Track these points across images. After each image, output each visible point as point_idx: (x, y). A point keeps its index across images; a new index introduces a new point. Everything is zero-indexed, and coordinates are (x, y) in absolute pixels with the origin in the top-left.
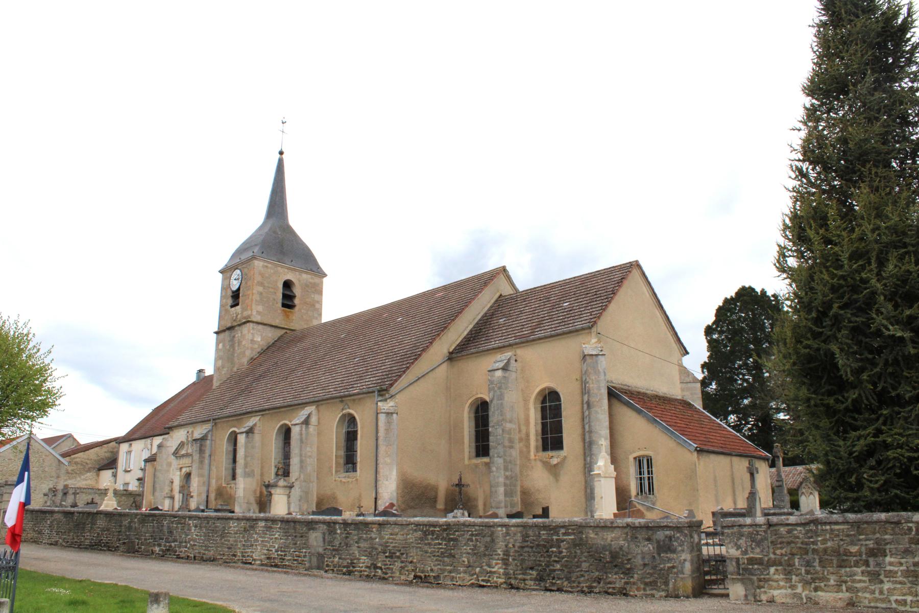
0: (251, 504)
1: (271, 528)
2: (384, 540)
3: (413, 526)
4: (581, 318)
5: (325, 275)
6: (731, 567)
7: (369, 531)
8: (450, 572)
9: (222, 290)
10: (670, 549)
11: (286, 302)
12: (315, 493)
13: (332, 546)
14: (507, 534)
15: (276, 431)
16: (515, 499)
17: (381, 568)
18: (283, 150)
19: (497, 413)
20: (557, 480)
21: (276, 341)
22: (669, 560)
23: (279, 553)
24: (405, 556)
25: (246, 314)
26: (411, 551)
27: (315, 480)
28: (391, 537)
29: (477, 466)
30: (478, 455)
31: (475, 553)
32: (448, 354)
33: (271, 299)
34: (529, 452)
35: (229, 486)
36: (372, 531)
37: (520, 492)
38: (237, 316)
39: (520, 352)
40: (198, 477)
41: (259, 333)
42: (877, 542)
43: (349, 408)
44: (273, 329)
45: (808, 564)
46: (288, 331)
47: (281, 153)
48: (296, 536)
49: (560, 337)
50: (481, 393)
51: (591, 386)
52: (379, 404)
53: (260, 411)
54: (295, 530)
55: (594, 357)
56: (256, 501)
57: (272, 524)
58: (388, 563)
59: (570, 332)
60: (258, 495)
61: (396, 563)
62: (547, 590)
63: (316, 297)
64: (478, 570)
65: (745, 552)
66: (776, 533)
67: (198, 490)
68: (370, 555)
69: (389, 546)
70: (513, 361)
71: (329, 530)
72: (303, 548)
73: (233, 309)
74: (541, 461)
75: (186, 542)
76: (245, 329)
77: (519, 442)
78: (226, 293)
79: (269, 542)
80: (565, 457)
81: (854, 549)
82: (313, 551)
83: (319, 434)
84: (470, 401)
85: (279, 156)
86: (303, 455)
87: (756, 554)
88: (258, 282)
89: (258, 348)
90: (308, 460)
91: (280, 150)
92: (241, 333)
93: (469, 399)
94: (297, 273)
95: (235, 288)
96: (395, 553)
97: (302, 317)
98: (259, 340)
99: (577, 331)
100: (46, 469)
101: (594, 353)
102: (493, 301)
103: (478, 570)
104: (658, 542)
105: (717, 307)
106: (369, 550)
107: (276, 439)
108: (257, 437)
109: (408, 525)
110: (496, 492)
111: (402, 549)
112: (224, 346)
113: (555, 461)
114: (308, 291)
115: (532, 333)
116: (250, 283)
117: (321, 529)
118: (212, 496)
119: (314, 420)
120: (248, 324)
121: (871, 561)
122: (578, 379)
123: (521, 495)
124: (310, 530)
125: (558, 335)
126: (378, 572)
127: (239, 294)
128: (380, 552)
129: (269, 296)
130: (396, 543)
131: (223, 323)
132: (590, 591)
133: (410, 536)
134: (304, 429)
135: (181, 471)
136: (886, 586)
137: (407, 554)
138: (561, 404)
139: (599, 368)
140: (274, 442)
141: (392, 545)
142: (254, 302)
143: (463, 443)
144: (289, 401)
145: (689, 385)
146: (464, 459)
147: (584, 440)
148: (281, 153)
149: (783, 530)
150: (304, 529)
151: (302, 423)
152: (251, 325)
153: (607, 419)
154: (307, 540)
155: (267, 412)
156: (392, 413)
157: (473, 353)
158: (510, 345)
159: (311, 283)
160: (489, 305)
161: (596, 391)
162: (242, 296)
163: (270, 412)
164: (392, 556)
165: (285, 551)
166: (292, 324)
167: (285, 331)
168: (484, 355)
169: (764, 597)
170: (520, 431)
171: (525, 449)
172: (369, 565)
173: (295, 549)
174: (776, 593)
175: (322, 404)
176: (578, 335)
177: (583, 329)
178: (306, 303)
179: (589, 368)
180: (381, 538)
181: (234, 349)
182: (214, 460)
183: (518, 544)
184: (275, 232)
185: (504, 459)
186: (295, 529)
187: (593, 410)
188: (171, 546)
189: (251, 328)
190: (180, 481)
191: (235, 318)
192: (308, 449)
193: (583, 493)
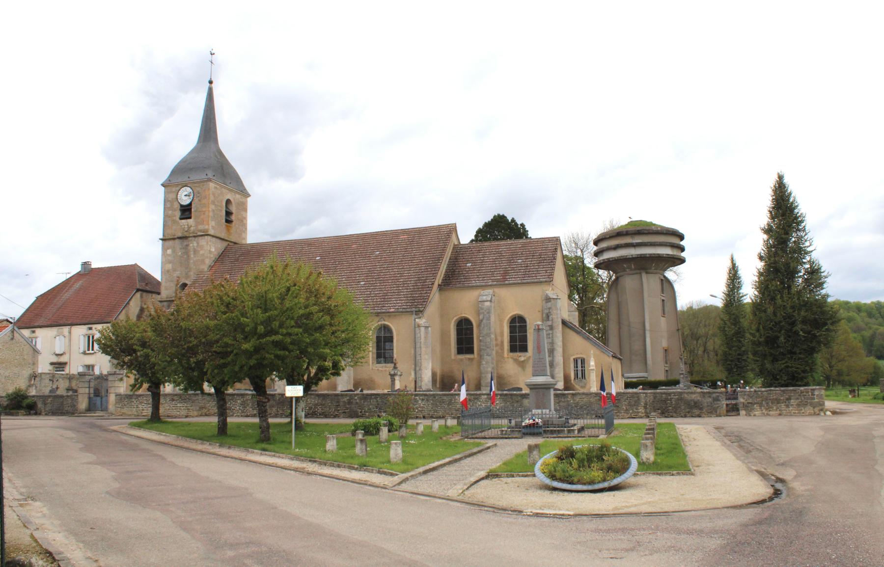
5: (249, 196)
6: (741, 405)
8: (616, 413)
10: (718, 400)
14: (646, 396)
18: (212, 79)
19: (486, 328)
20: (524, 370)
22: (718, 404)
25: (201, 227)
29: (462, 360)
30: (460, 351)
31: (630, 404)
34: (503, 353)
39: (497, 290)
42: (789, 396)
44: (221, 241)
45: (767, 403)
46: (230, 244)
47: (211, 82)
52: (417, 320)
62: (666, 417)
64: (631, 411)
65: (746, 400)
66: (757, 394)
74: (512, 358)
76: (203, 241)
81: (782, 398)
84: (455, 318)
87: (750, 401)
91: (209, 79)
92: (198, 243)
99: (541, 282)
100: (25, 357)
103: (631, 411)
104: (713, 398)
105: (477, 229)
110: (486, 377)
112: (174, 252)
113: (522, 359)
116: (204, 201)
120: (206, 237)
121: (787, 402)
127: (191, 209)
131: (169, 231)
132: (685, 416)
136: (791, 408)
142: (210, 218)
145: (572, 313)
148: (211, 82)
149: (760, 393)
156: (428, 327)
162: (196, 211)
169: (752, 414)
170: (496, 339)
171: (500, 351)
174: (756, 413)
177: (546, 282)
180: (574, 400)
181: (188, 256)
183: (651, 400)
186: (512, 399)
187: (554, 331)
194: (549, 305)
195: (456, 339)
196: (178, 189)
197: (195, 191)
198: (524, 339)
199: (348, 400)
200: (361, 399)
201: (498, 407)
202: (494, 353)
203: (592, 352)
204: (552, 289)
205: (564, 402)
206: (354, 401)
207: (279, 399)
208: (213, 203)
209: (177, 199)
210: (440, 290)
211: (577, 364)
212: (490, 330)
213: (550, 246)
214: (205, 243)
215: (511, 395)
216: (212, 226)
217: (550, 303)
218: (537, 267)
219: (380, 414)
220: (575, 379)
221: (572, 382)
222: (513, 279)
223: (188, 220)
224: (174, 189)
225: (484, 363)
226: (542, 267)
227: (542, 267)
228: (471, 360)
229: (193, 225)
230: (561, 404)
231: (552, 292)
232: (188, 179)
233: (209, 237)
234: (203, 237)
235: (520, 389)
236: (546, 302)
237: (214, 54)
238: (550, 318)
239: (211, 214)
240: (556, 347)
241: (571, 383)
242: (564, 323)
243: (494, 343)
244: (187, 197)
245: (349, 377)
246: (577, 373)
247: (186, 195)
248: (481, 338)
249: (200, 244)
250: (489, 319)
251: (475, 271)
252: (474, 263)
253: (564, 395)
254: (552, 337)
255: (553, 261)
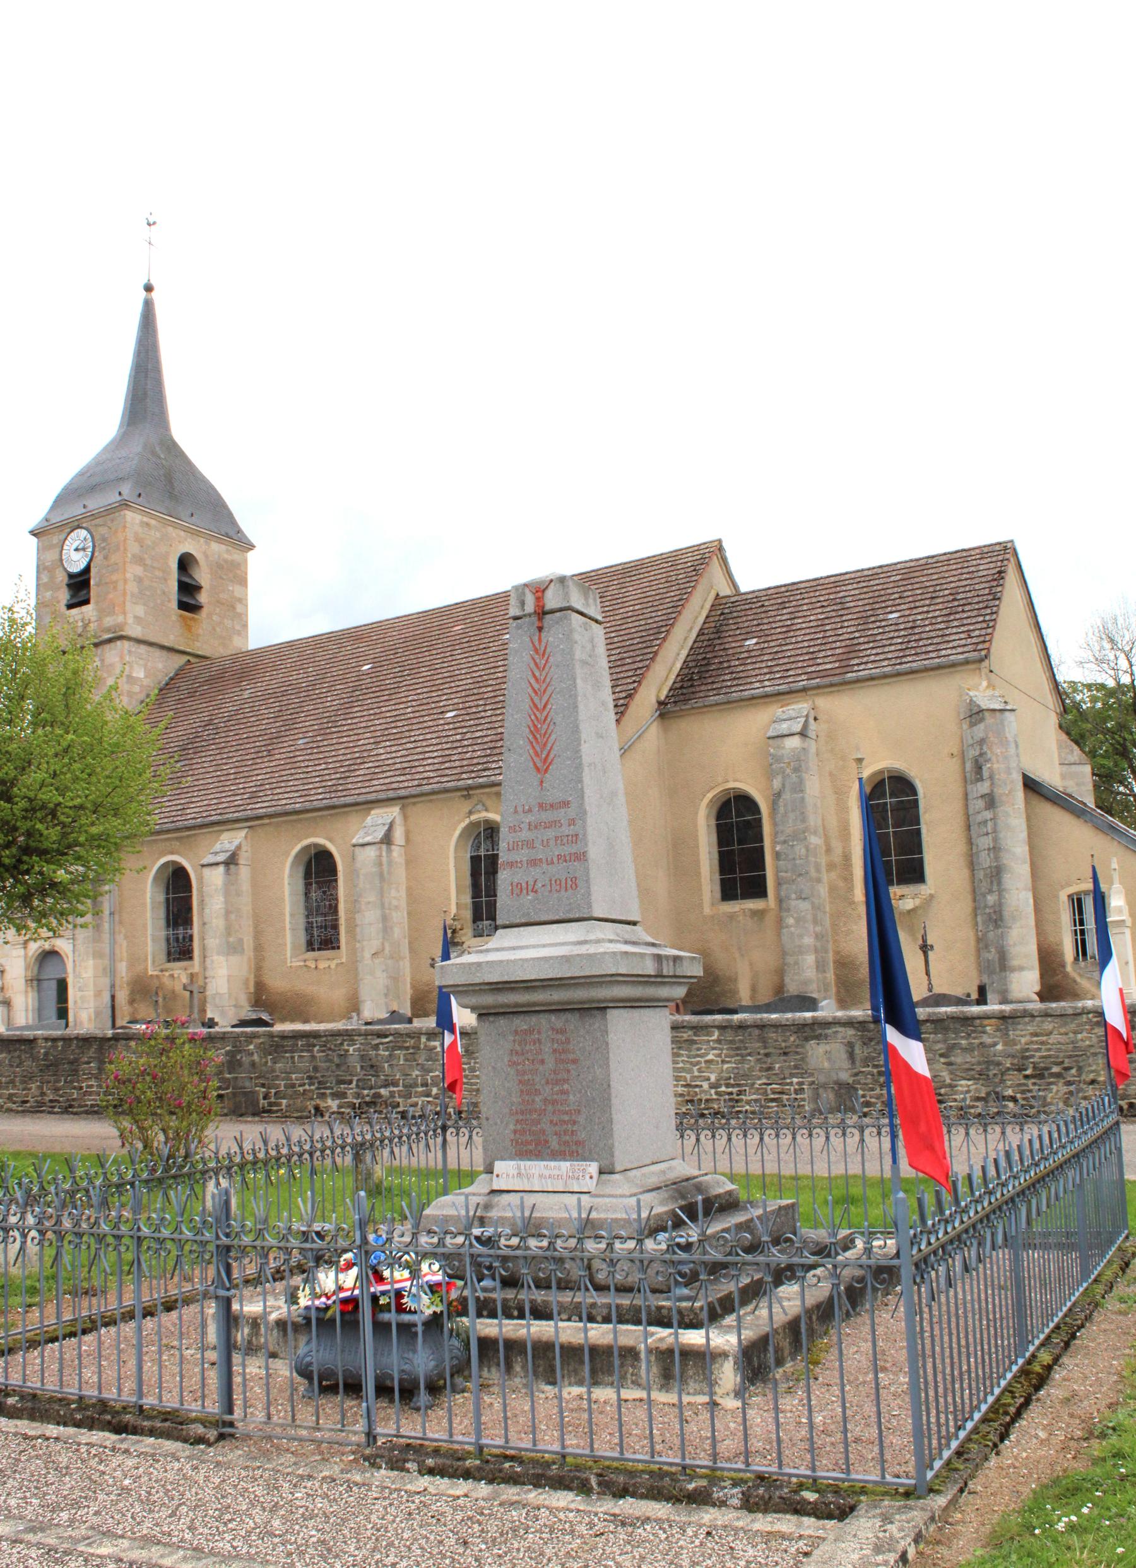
0: (242, 1007)
1: (693, 1042)
2: (1018, 1047)
3: (1090, 1016)
4: (948, 642)
5: (251, 547)
7: (974, 1031)
9: (38, 572)
11: (185, 599)
12: (408, 980)
13: (875, 1066)
15: (290, 859)
16: (828, 975)
17: (1014, 1099)
18: (153, 282)
19: (792, 816)
21: (172, 679)
23: (723, 1089)
24: (1073, 1071)
25: (108, 621)
26: (1091, 1060)
27: (407, 955)
28: (1035, 1039)
29: (732, 917)
30: (728, 892)
32: (656, 706)
33: (159, 592)
34: (851, 889)
35: (167, 974)
36: (984, 1032)
37: (834, 962)
38: (85, 626)
39: (824, 703)
40: (94, 958)
41: (141, 662)
43: (487, 810)
44: (164, 653)
46: (193, 660)
47: (149, 288)
48: (767, 1055)
49: (931, 673)
50: (735, 780)
51: (995, 766)
53: (247, 820)
54: (764, 1042)
55: (998, 714)
56: (249, 1000)
57: (695, 1035)
58: (1031, 1087)
59: (939, 667)
60: (252, 990)
61: (1054, 1088)
63: (237, 590)
67: (95, 985)
68: (982, 1076)
69: (1032, 1056)
70: (811, 720)
71: (862, 1037)
72: (792, 1075)
73: (74, 611)
75: (425, 1085)
76: (113, 654)
77: (828, 871)
78: (52, 578)
79: (690, 1071)
80: (932, 896)
82: (822, 1079)
83: (408, 863)
84: (710, 796)
85: (143, 294)
86: (386, 905)
88: (134, 556)
89: (140, 692)
90: (394, 914)
92: (102, 661)
93: (709, 791)
94: (202, 540)
95: (76, 568)
96: (1047, 1069)
97: (214, 629)
98: (142, 675)
99: (953, 665)
101: (997, 707)
102: (708, 606)
106: (978, 1068)
107: (291, 876)
108: (244, 872)
109: (1080, 1014)
110: (796, 963)
111: (1067, 1060)
114: (221, 578)
115: (847, 667)
116: (114, 558)
117: (840, 1036)
118: (122, 997)
119: (399, 835)
120: (119, 643)
122: (955, 753)
123: (835, 968)
124: (807, 1039)
125: (899, 674)
126: (1006, 1106)
128: (1008, 1069)
129: (155, 584)
130: (1049, 1050)
133: (1085, 1034)
134: (384, 854)
135: (25, 948)
137: (1080, 1069)
138: (916, 801)
139: (1008, 735)
140: (286, 881)
141: (1038, 1054)
142: (128, 598)
143: (698, 874)
144: (318, 798)
145: (1074, 768)
146: (701, 905)
147: (972, 864)
148: (149, 288)
150: (792, 1039)
151: (381, 842)
152: (126, 644)
153: (1024, 826)
154: (802, 1059)
155: (266, 821)
157: (717, 704)
158: (804, 690)
159: (226, 561)
160: (704, 613)
161: (1003, 776)
162: (98, 585)
163: (273, 820)
164: (1040, 1074)
165: (739, 1085)
166: (198, 644)
167: (186, 658)
168: (741, 707)
170: (829, 850)
171: (841, 884)
172: (983, 1095)
173: (768, 1079)
175: (414, 804)
176: (951, 673)
177: (967, 662)
178: (219, 602)
179: (990, 735)
182: (121, 922)
184: (153, 453)
185: (813, 903)
186: (764, 1041)
187: (1001, 810)
188: (378, 1095)
189: (126, 652)
190: (27, 968)
191: (80, 630)
192: (393, 893)
193: (972, 959)
194: (979, 731)
195: (716, 856)
196: (63, 536)
197: (97, 537)
198: (912, 843)
199: (227, 1053)
200: (265, 1051)
201: (713, 1078)
202: (823, 890)
203: (1115, 865)
204: (990, 686)
205: (969, 1049)
206: (246, 1060)
207: (46, 1054)
208: (139, 560)
209: (61, 560)
210: (662, 716)
211: (1081, 912)
212: (804, 820)
213: (986, 568)
214: (117, 659)
215: (762, 1026)
216: (136, 617)
217: (982, 726)
218: (942, 626)
219: (322, 1105)
220: (1076, 959)
221: (1069, 968)
222: (870, 666)
223: (85, 608)
224: (55, 540)
225: (791, 921)
226: (956, 623)
227: (956, 623)
228: (759, 914)
229: (93, 619)
230: (958, 1058)
231: (989, 692)
232: (84, 511)
233: (126, 644)
234: (112, 645)
235: (810, 1003)
236: (972, 725)
237: (154, 223)
238: (986, 774)
239: (132, 587)
240: (1006, 859)
241: (1066, 975)
242: (1031, 786)
243: (823, 860)
244: (81, 553)
245: (395, 979)
246: (1083, 941)
247: (77, 550)
248: (778, 848)
249: (108, 661)
250: (799, 787)
251: (766, 658)
252: (763, 636)
253: (967, 1020)
254: (995, 831)
255: (991, 603)
